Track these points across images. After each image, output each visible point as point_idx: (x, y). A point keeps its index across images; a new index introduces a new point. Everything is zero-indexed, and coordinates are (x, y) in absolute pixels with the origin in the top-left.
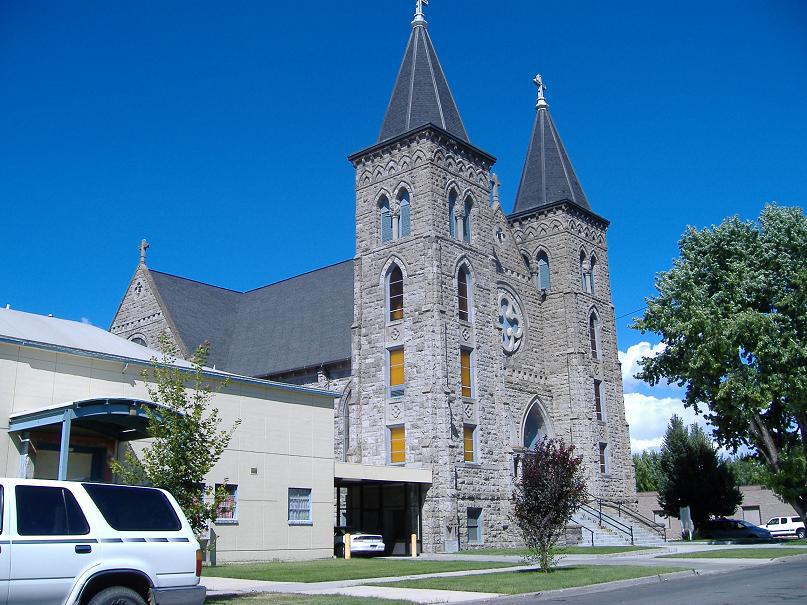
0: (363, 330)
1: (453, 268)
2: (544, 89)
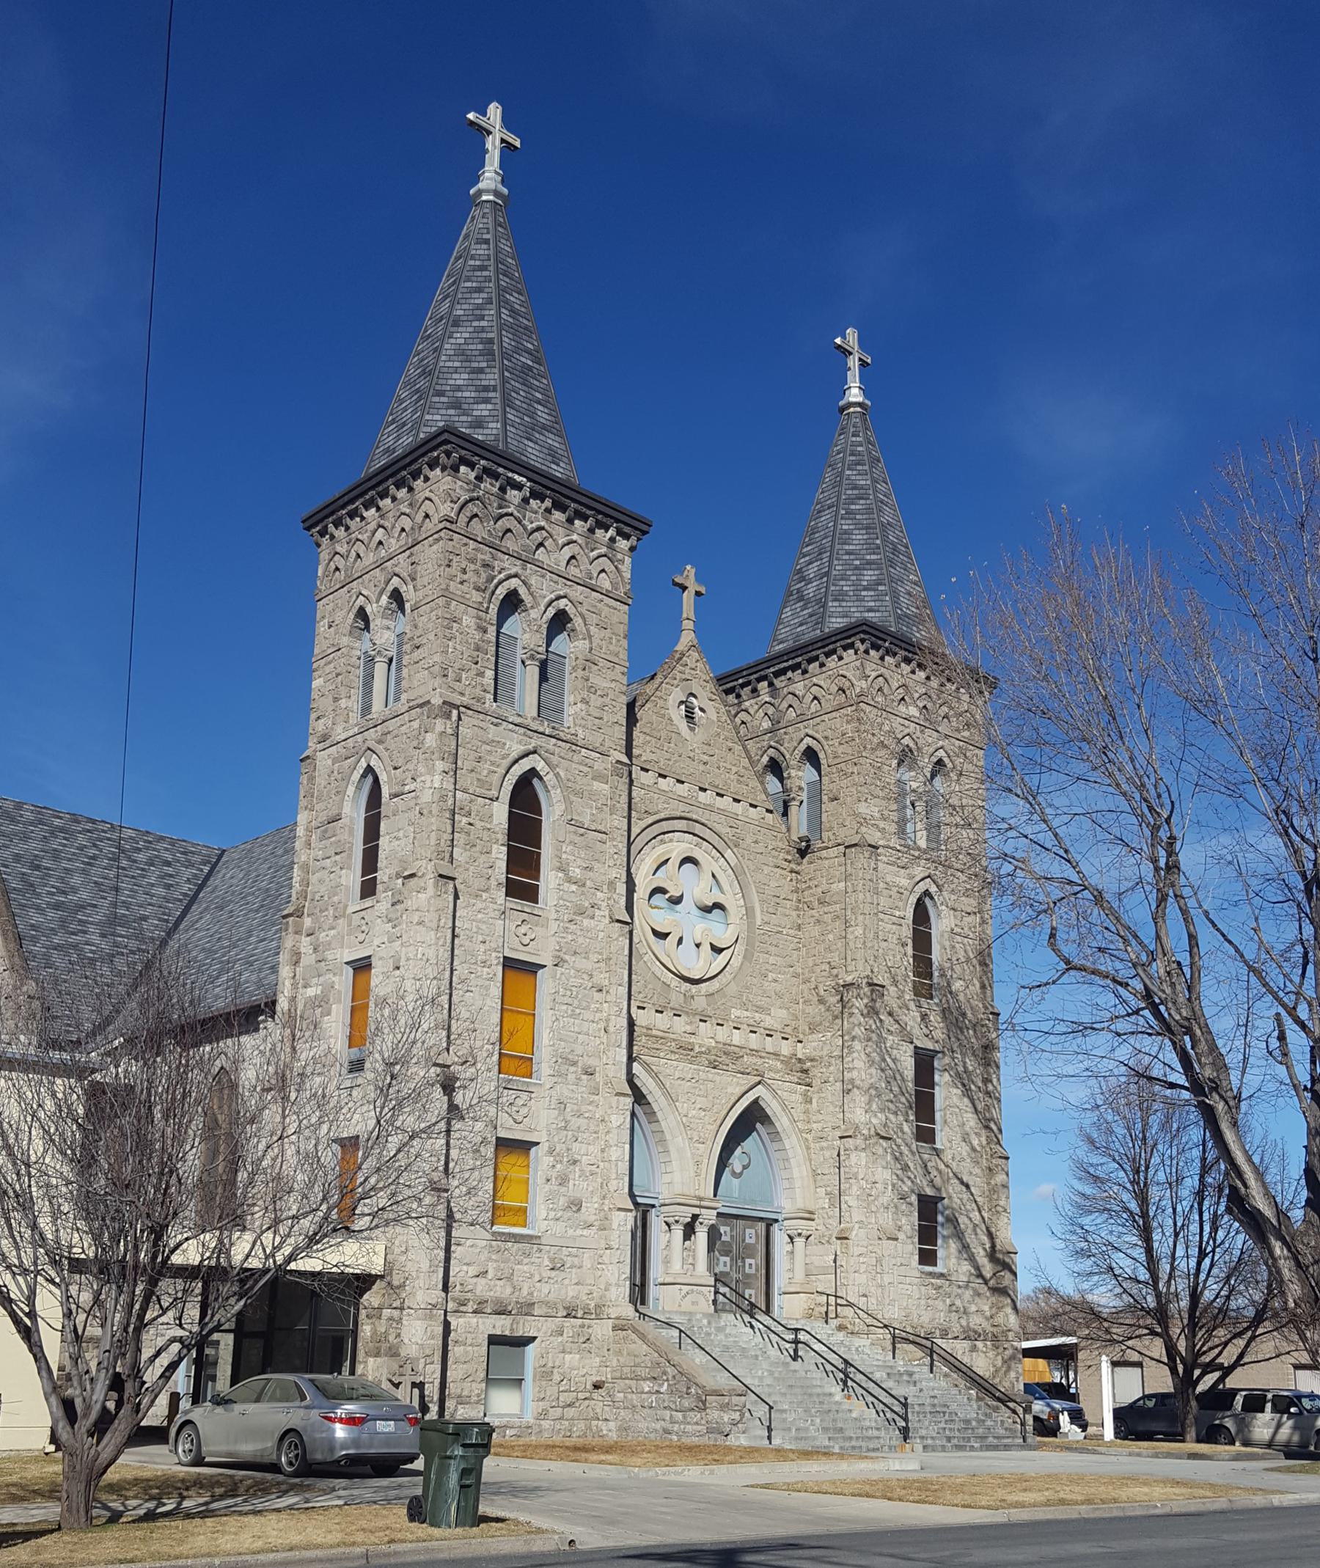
0: (307, 922)
1: (496, 779)
2: (863, 364)
